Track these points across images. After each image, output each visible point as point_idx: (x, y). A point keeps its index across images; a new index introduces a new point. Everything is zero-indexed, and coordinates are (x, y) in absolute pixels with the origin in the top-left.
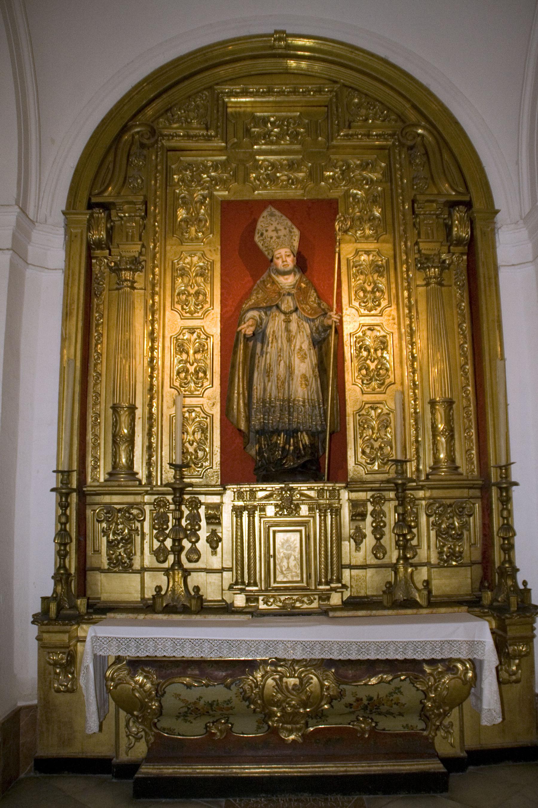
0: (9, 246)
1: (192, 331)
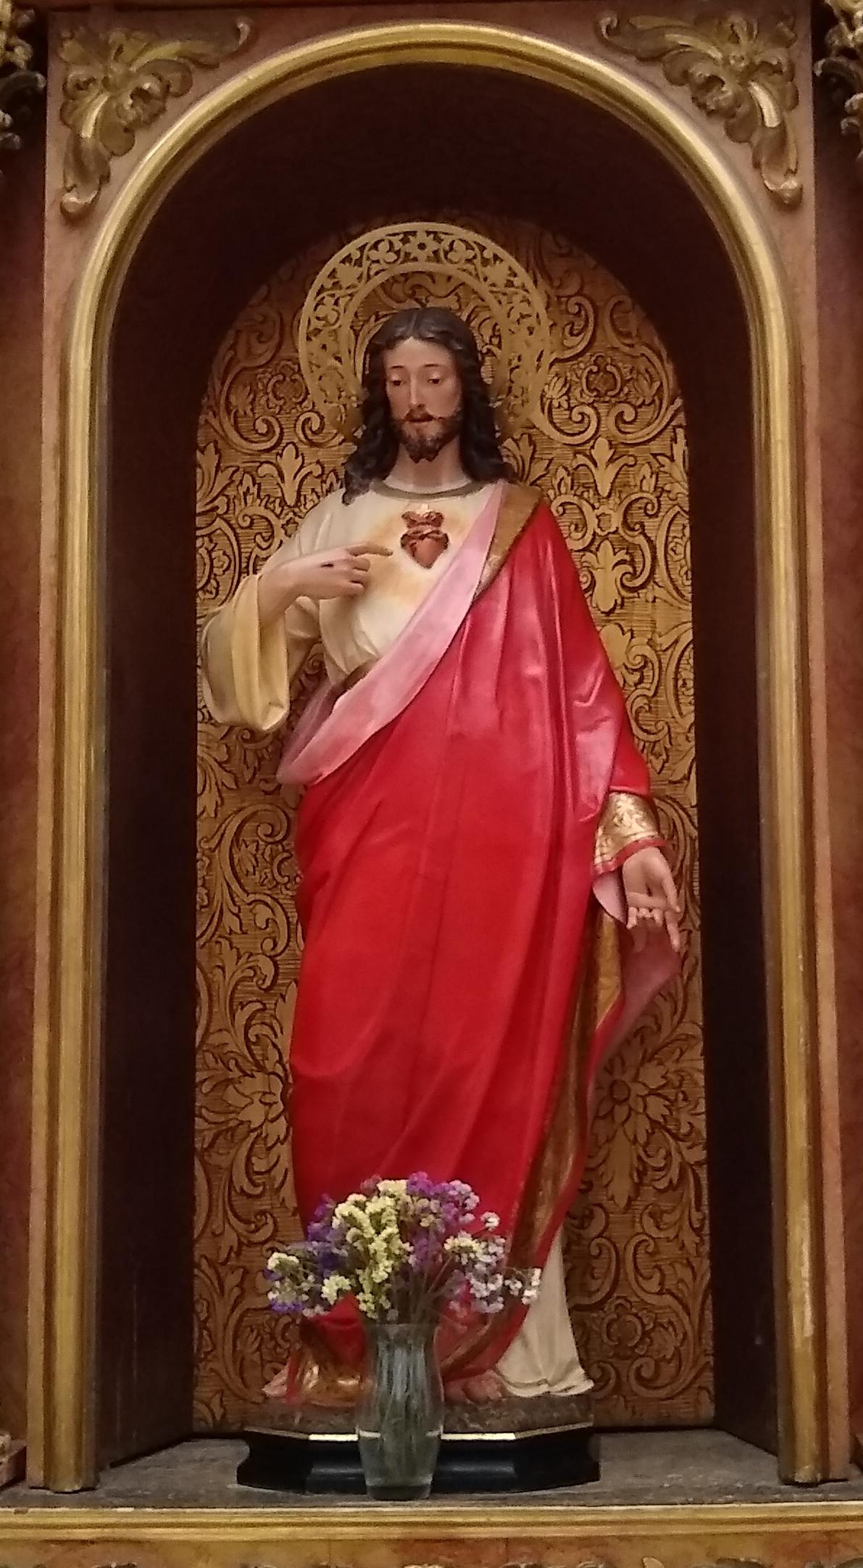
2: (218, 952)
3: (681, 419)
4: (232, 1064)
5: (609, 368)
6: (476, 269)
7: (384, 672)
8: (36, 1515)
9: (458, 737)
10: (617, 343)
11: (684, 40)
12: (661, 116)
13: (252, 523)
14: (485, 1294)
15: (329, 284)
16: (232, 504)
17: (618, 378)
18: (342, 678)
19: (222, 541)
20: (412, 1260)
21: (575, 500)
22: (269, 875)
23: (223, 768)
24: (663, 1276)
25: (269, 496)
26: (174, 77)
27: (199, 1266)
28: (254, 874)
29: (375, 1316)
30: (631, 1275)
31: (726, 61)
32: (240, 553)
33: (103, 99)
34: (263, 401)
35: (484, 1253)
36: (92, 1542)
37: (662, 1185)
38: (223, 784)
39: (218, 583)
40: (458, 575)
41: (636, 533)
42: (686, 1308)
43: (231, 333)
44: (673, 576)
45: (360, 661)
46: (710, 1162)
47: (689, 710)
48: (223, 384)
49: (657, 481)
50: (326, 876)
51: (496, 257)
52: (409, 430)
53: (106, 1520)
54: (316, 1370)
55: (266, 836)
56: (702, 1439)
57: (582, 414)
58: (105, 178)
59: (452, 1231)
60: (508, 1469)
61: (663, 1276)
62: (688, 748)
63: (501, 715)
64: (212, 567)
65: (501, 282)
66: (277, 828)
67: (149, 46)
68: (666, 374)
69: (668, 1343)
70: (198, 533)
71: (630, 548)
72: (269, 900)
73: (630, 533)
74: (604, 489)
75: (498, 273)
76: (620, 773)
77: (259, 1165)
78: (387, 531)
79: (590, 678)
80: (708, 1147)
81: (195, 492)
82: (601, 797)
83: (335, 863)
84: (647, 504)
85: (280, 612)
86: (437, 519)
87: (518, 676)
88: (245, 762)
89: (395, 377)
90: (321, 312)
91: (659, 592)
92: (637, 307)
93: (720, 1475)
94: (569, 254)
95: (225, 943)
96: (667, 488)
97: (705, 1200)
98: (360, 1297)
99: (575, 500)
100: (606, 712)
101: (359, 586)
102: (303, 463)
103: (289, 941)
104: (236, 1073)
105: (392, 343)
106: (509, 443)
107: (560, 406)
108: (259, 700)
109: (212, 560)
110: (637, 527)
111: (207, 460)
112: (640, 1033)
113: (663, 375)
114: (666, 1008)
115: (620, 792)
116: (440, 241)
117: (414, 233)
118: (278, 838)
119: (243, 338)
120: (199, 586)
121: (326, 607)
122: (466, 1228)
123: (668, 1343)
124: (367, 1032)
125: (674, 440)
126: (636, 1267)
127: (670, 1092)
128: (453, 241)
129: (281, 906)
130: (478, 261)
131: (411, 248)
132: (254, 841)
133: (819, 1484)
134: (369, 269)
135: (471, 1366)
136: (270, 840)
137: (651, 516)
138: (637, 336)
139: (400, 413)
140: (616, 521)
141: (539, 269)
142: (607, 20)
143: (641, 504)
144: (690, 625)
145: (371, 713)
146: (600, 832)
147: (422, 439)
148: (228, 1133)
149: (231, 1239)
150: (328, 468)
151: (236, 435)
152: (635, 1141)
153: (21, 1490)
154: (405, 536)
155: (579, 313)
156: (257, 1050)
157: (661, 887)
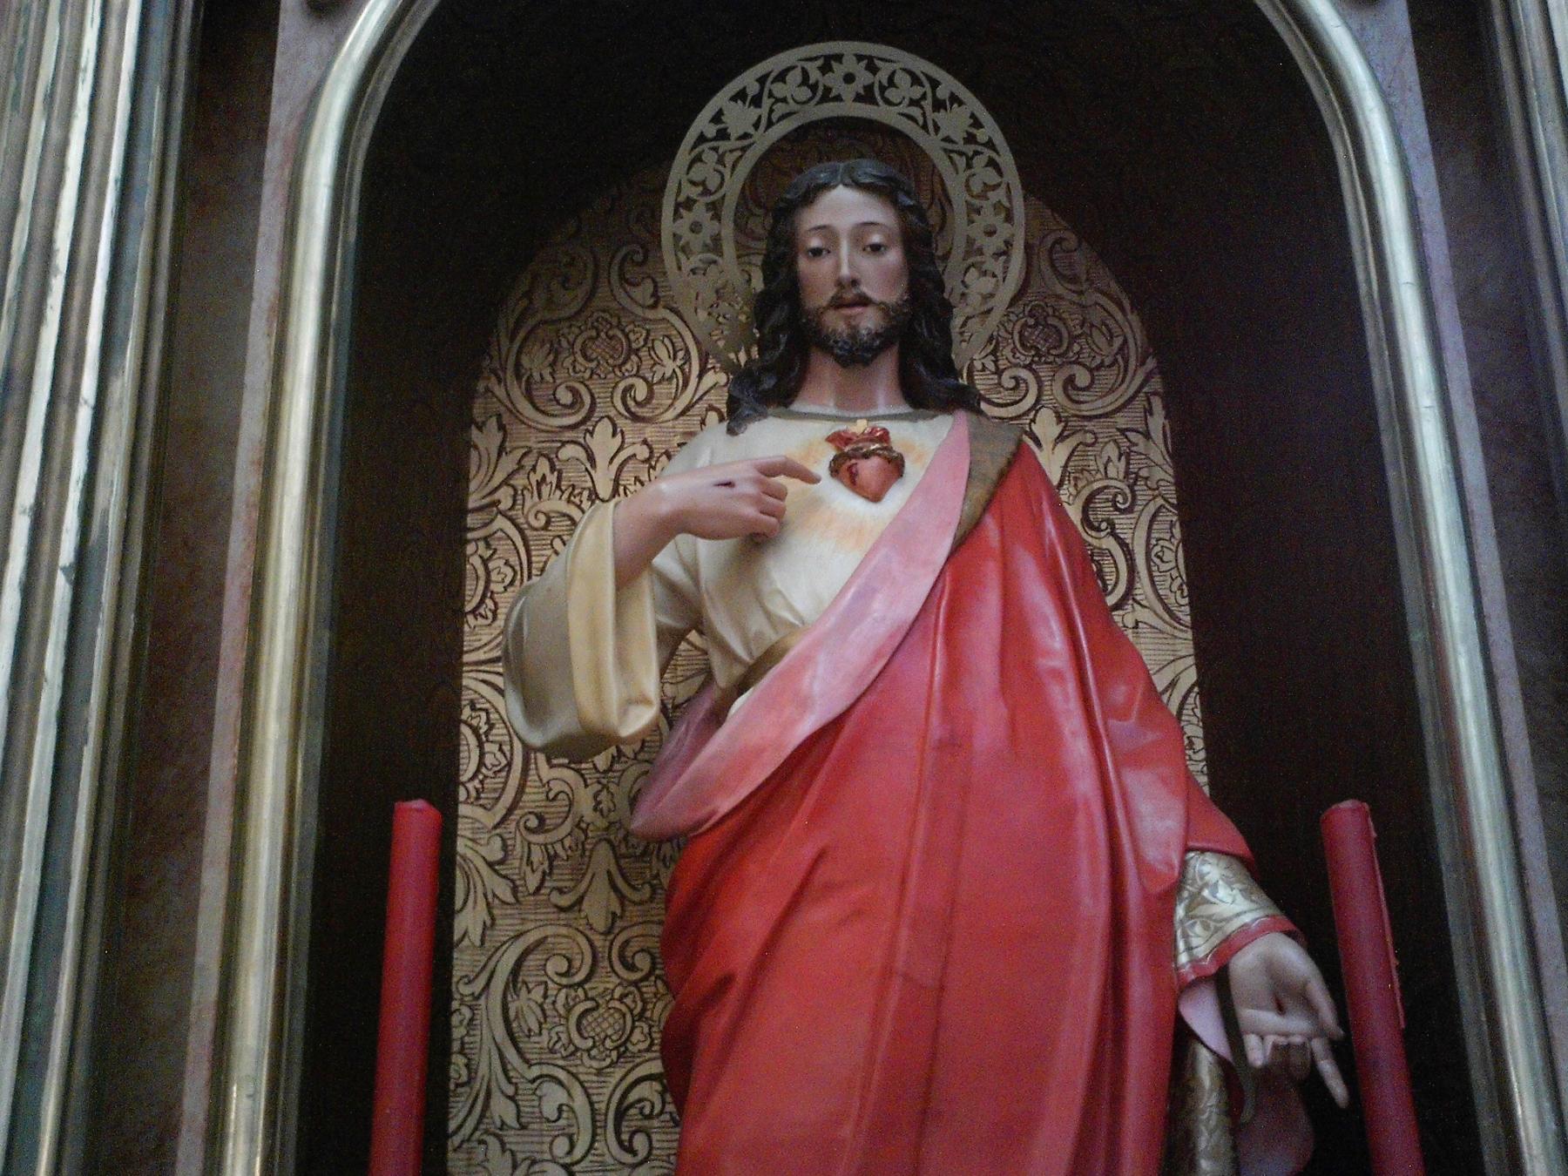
0: (655, 387)
1: (461, 1022)
2: (481, 1157)
3: (1156, 384)
5: (1051, 321)
6: (924, 114)
10: (1060, 290)
13: (548, 522)
16: (520, 497)
17: (1066, 335)
18: (738, 671)
19: (503, 548)
22: (564, 1036)
23: (496, 872)
25: (574, 487)
28: (540, 1034)
32: (530, 563)
34: (568, 363)
38: (495, 895)
39: (496, 604)
41: (1103, 534)
44: (1161, 592)
45: (771, 636)
48: (512, 340)
49: (1128, 463)
50: (726, 982)
51: (954, 99)
52: (835, 322)
55: (558, 974)
57: (1016, 378)
64: (488, 581)
65: (959, 136)
66: (577, 964)
68: (1131, 327)
70: (470, 535)
72: (562, 1075)
73: (1094, 533)
75: (954, 123)
81: (468, 481)
83: (742, 959)
84: (1115, 496)
88: (530, 863)
89: (815, 243)
90: (698, 173)
91: (1143, 615)
92: (1084, 244)
95: (493, 1143)
96: (1144, 473)
101: (773, 520)
102: (623, 442)
103: (593, 1141)
107: (984, 368)
108: (614, 693)
109: (488, 572)
110: (1104, 525)
111: (485, 440)
113: (1127, 330)
115: (1203, 851)
117: (839, 58)
118: (577, 979)
120: (468, 608)
121: (708, 554)
125: (1149, 411)
128: (894, 73)
129: (581, 1083)
131: (834, 80)
132: (540, 983)
134: (771, 111)
136: (564, 981)
137: (1122, 511)
138: (1087, 280)
144: (1191, 660)
145: (804, 704)
147: (854, 333)
151: (530, 406)
154: (835, 459)
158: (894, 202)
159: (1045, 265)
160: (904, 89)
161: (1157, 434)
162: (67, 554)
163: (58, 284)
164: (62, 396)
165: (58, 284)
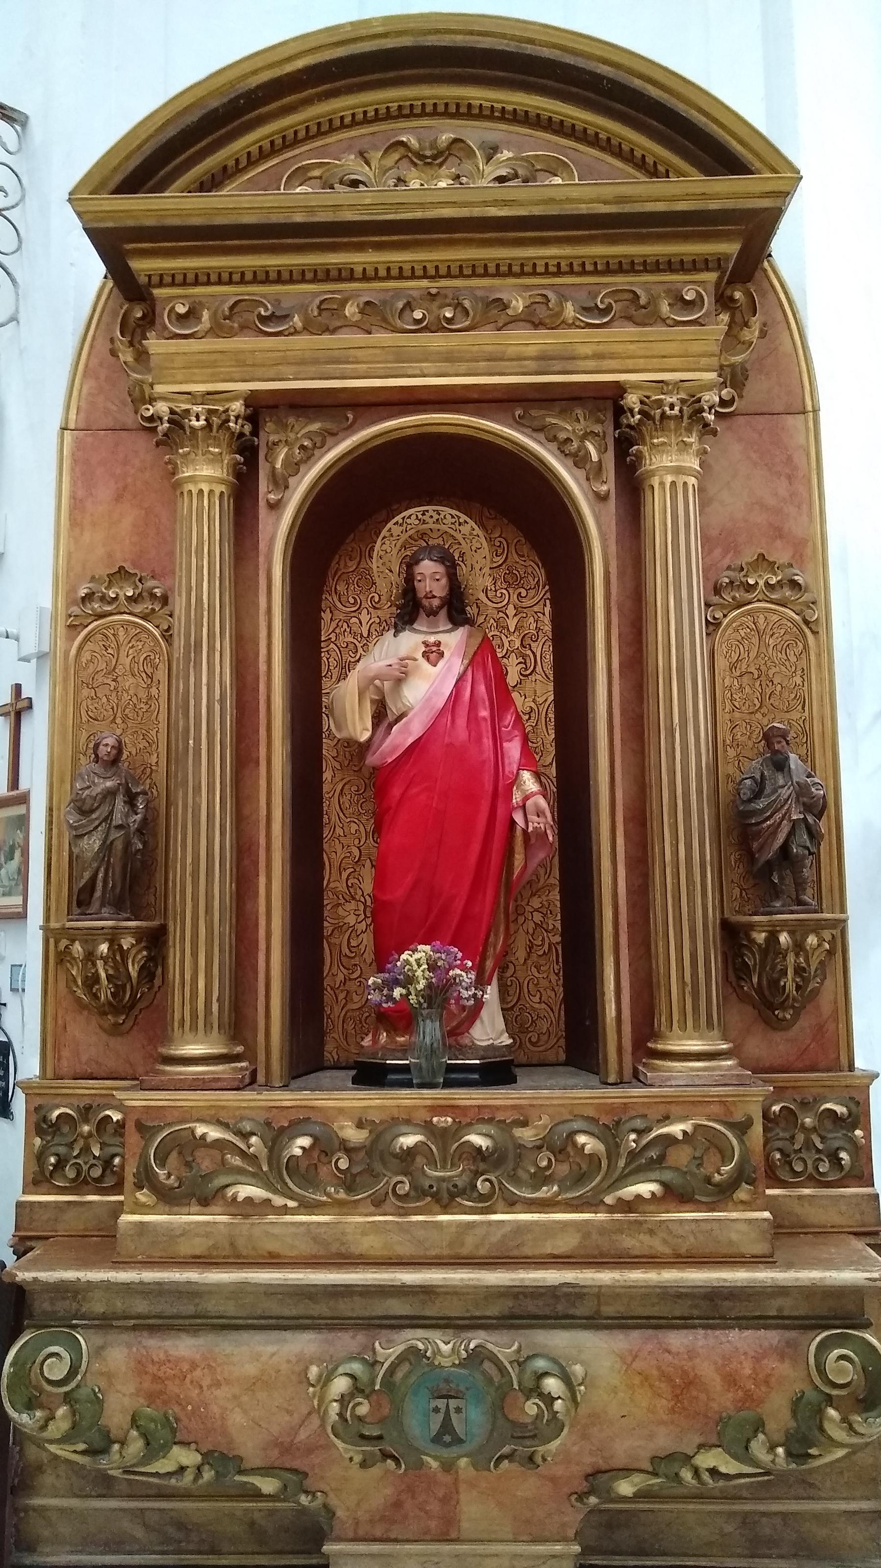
3: (548, 595)
4: (340, 896)
7: (415, 715)
8: (266, 1095)
9: (450, 745)
11: (554, 421)
12: (551, 464)
14: (467, 996)
15: (387, 534)
19: (333, 654)
20: (433, 980)
21: (498, 634)
24: (541, 995)
26: (318, 440)
27: (326, 990)
29: (417, 1006)
30: (527, 996)
31: (574, 430)
33: (286, 450)
35: (468, 978)
36: (291, 1107)
37: (541, 953)
40: (449, 669)
42: (552, 1010)
43: (337, 556)
46: (562, 942)
47: (552, 733)
50: (390, 808)
51: (466, 522)
52: (425, 602)
53: (298, 1097)
54: (385, 1034)
56: (561, 1068)
58: (287, 487)
59: (452, 968)
60: (476, 1076)
61: (541, 995)
62: (552, 750)
63: (470, 735)
67: (306, 425)
69: (544, 1026)
71: (524, 656)
74: (512, 630)
75: (465, 529)
76: (523, 761)
77: (354, 943)
78: (416, 649)
79: (509, 717)
80: (562, 935)
82: (515, 772)
85: (367, 687)
86: (438, 644)
87: (476, 718)
90: (384, 546)
91: (538, 677)
93: (571, 1081)
94: (495, 518)
97: (560, 960)
98: (410, 997)
99: (498, 634)
100: (516, 733)
104: (343, 901)
105: (417, 562)
106: (468, 608)
108: (359, 728)
111: (326, 616)
112: (530, 883)
114: (542, 871)
116: (439, 514)
117: (427, 511)
119: (343, 557)
121: (387, 685)
122: (458, 967)
123: (544, 1026)
124: (409, 879)
125: (545, 605)
126: (529, 991)
127: (544, 910)
130: (457, 524)
133: (620, 1083)
135: (458, 1031)
139: (421, 594)
140: (518, 644)
141: (482, 525)
142: (518, 412)
143: (529, 635)
145: (410, 734)
146: (515, 788)
148: (338, 928)
149: (341, 977)
150: (383, 619)
152: (528, 932)
153: (255, 1086)
155: (499, 546)
156: (352, 890)
157: (544, 814)
158: (443, 563)
159: (514, 551)
160: (449, 519)
161: (547, 614)
162: (217, 697)
163: (206, 613)
164: (212, 648)
165: (206, 613)
